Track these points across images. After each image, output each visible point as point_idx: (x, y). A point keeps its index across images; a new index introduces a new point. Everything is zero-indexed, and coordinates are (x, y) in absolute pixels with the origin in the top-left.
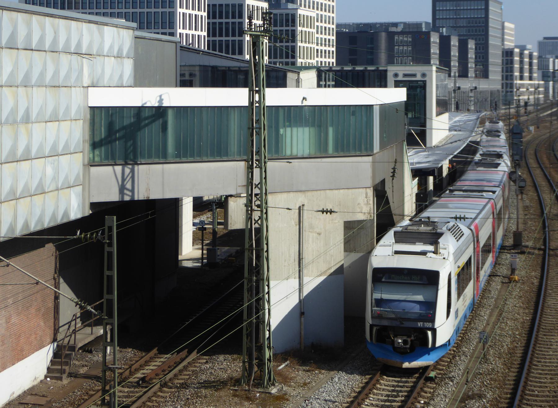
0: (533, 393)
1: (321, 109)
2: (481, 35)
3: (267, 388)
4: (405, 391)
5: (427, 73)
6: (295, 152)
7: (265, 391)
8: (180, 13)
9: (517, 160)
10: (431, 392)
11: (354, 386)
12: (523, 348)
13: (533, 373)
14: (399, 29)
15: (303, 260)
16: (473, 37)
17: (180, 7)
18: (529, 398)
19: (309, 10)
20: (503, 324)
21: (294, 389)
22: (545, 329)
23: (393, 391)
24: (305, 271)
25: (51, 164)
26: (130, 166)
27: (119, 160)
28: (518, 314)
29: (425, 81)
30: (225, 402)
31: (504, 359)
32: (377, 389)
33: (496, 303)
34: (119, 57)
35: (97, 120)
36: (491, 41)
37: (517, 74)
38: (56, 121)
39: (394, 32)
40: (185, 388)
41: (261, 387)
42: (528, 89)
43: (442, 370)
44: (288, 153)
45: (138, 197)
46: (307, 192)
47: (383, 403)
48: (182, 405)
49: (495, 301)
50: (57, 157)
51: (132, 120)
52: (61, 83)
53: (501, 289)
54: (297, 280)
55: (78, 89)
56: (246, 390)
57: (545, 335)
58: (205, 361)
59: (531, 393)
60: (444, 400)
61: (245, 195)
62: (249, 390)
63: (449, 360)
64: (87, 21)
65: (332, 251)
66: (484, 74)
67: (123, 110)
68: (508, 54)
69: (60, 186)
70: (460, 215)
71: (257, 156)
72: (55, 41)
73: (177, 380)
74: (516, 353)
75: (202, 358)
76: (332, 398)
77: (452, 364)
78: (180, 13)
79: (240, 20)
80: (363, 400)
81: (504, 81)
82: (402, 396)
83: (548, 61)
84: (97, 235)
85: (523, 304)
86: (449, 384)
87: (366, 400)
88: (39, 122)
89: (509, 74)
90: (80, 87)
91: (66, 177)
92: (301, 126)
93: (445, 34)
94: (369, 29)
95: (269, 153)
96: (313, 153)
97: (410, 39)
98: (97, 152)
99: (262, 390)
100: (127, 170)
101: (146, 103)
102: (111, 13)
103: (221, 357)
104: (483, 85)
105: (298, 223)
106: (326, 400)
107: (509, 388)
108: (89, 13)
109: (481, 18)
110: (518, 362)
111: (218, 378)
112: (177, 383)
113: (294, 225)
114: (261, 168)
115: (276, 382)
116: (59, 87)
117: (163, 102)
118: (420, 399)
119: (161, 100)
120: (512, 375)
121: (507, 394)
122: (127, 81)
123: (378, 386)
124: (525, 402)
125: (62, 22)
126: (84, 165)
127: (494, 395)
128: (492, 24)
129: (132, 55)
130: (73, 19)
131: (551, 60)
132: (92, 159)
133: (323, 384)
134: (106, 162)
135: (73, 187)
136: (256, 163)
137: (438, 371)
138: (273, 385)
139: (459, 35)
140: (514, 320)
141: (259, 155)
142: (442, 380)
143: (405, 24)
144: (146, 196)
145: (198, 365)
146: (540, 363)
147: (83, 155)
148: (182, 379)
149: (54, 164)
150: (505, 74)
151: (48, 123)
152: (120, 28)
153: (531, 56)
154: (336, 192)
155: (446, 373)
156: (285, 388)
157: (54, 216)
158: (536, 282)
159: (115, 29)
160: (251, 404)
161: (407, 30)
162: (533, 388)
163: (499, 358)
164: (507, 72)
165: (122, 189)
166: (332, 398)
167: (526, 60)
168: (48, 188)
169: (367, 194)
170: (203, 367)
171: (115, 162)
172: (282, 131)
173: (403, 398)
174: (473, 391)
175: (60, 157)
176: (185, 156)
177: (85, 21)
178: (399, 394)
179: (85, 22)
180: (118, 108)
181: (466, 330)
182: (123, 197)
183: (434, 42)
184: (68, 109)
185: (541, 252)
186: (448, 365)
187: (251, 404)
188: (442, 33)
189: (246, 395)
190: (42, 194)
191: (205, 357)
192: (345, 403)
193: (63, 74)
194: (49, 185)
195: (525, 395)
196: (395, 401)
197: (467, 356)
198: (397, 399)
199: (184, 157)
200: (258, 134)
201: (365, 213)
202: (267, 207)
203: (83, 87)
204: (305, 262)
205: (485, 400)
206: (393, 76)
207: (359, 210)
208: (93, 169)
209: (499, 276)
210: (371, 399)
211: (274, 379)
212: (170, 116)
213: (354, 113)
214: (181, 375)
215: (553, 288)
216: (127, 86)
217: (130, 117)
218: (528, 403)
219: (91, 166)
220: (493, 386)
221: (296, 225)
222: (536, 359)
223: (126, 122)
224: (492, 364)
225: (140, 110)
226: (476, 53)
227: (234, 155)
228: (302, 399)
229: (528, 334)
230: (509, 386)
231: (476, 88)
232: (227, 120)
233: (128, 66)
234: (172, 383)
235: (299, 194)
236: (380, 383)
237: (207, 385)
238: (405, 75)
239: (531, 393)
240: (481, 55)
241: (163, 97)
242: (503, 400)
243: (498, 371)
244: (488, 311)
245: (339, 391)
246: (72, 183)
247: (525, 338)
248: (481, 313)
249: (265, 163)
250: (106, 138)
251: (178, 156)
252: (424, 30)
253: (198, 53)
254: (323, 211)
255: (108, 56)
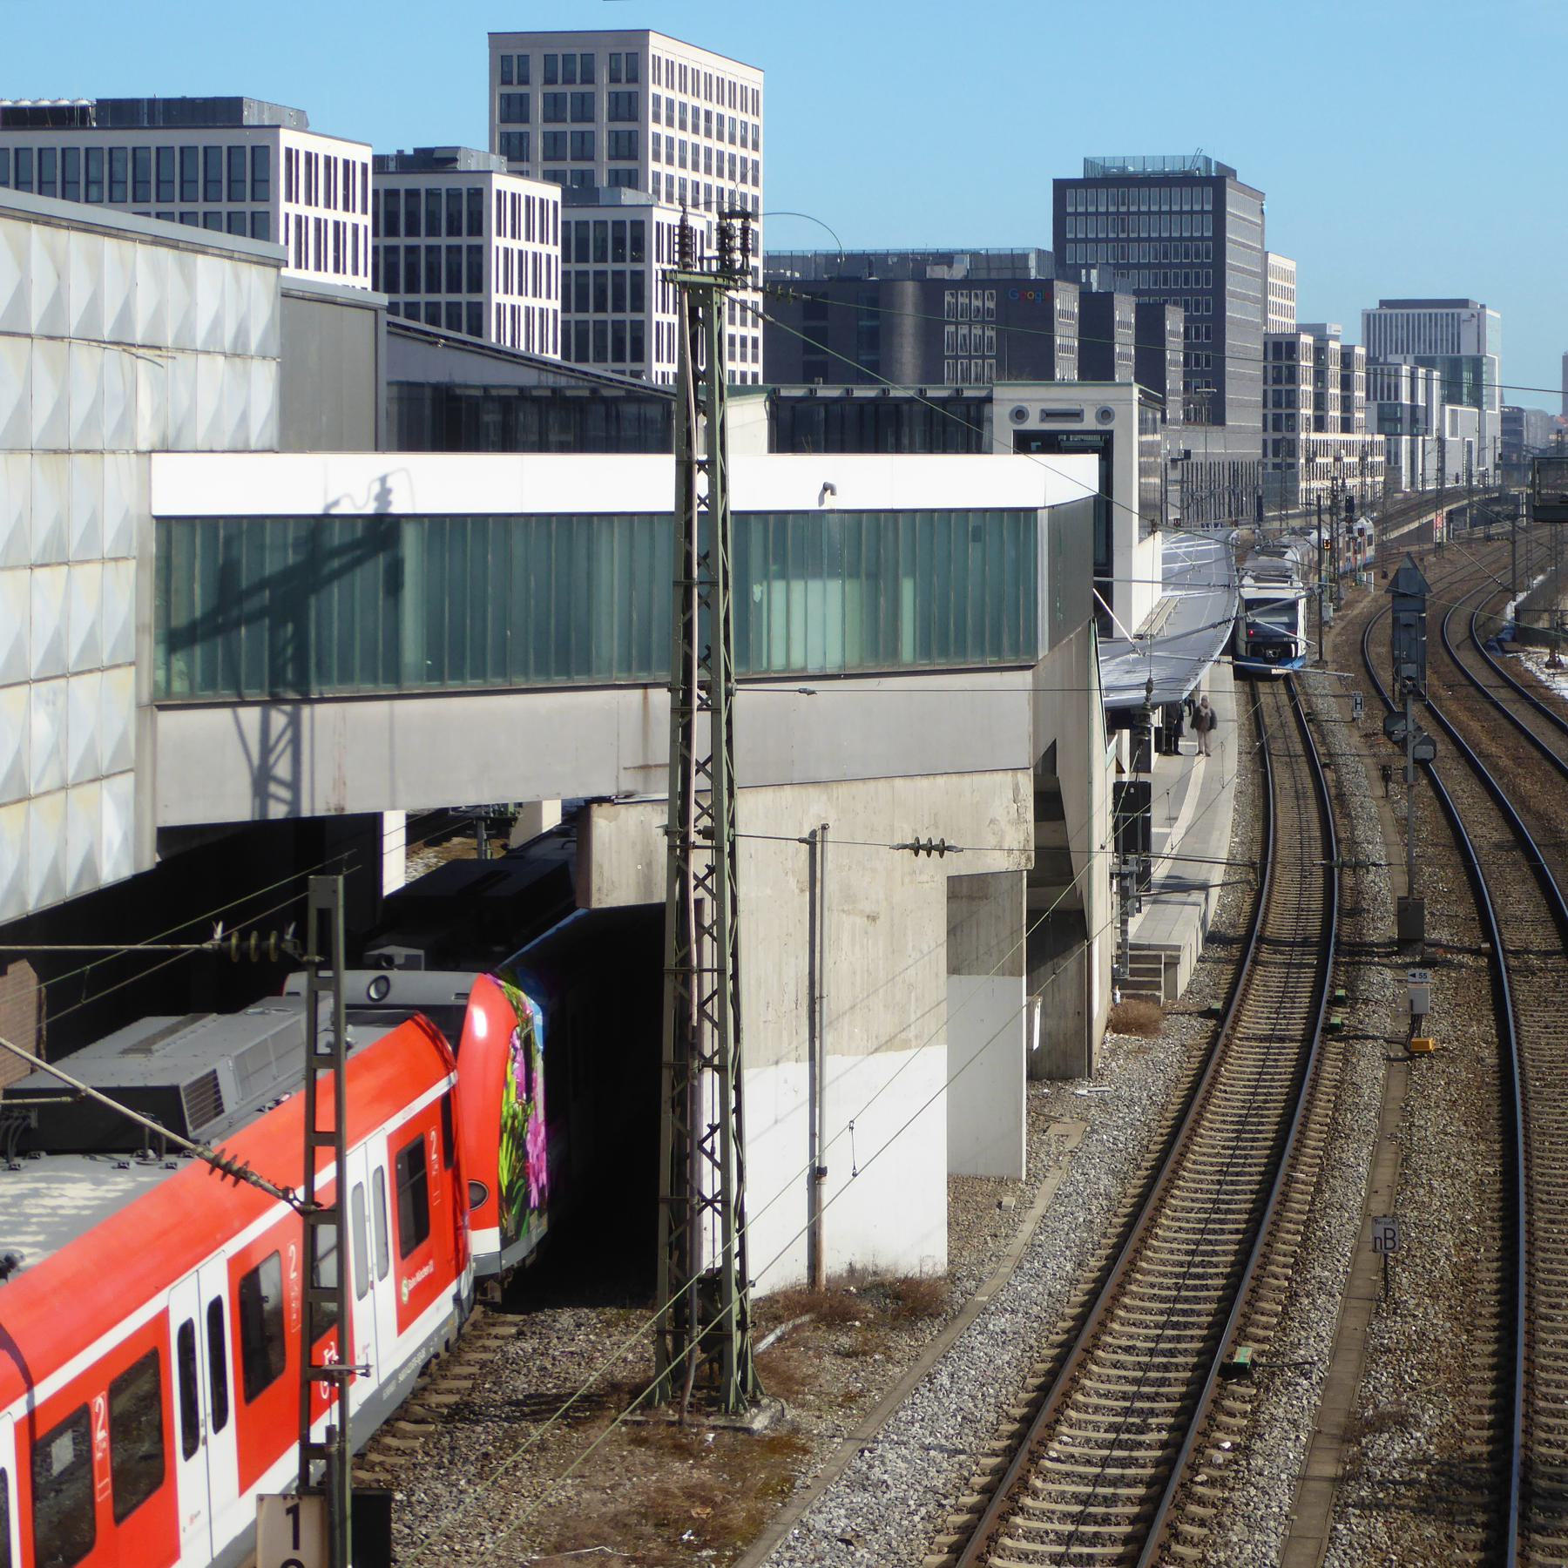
0: (1559, 1406)
1: (878, 520)
2: (1202, 292)
3: (736, 1413)
4: (1165, 1412)
5: (1117, 409)
6: (797, 660)
7: (732, 1424)
8: (287, 216)
9: (1409, 678)
10: (1246, 1412)
11: (1002, 1399)
12: (1495, 1264)
13: (1545, 1342)
14: (959, 271)
15: (825, 1000)
16: (1175, 297)
17: (289, 199)
18: (1552, 1421)
19: (669, 206)
20: (1422, 1192)
21: (817, 1413)
22: (1550, 1202)
23: (1127, 1412)
24: (829, 1038)
25: (47, 703)
26: (288, 708)
27: (248, 687)
28: (1460, 1156)
29: (1111, 433)
30: (609, 1461)
31: (1449, 1299)
32: (1077, 1407)
33: (1382, 1123)
34: (239, 356)
35: (179, 559)
36: (1234, 311)
37: (1306, 411)
38: (60, 564)
39: (943, 280)
40: (464, 1420)
41: (719, 1410)
42: (1338, 459)
43: (1266, 1340)
44: (778, 661)
45: (313, 810)
46: (834, 785)
47: (1106, 1452)
48: (470, 1476)
49: (1378, 1116)
50: (62, 682)
51: (291, 559)
52: (75, 440)
53: (1387, 1078)
54: (806, 1065)
55: (121, 457)
56: (671, 1424)
57: (1552, 1222)
58: (513, 1330)
59: (1552, 1406)
60: (1293, 1437)
61: (666, 796)
62: (680, 1422)
63: (1280, 1308)
64: (149, 238)
65: (911, 971)
66: (1212, 411)
67: (263, 528)
68: (1281, 350)
69: (71, 773)
70: (930, 840)
71: (704, 671)
72: (58, 302)
73: (435, 1395)
74: (1481, 1282)
75: (502, 1319)
76: (943, 1442)
77: (1292, 1319)
78: (287, 216)
79: (475, 241)
80: (1042, 1443)
81: (1272, 435)
82: (1160, 1429)
83: (1398, 375)
84: (281, 938)
85: (1465, 1124)
86: (1298, 1384)
87: (1050, 1444)
88: (12, 568)
89: (1284, 411)
90: (128, 452)
91: (91, 749)
92: (817, 575)
93: (1095, 287)
94: (867, 270)
95: (738, 663)
96: (853, 666)
97: (991, 305)
98: (179, 664)
99: (721, 1422)
100: (279, 719)
101: (336, 503)
102: (205, 214)
103: (566, 1318)
104: (1210, 446)
105: (807, 885)
106: (927, 1448)
107: (1482, 1391)
108: (158, 216)
109: (1202, 238)
110: (1493, 1310)
111: (568, 1385)
112: (438, 1406)
113: (797, 891)
114: (716, 712)
115: (762, 1393)
116: (68, 452)
117: (392, 497)
118: (1219, 1435)
119: (384, 495)
120: (1483, 1351)
121: (1481, 1413)
122: (261, 434)
123: (1080, 1397)
124: (1543, 1435)
125: (76, 241)
126: (139, 706)
127: (1441, 1414)
128: (1233, 258)
129: (274, 349)
130: (108, 231)
131: (1405, 370)
132: (162, 684)
133: (904, 1396)
134: (208, 696)
135: (107, 777)
136: (699, 697)
137: (1256, 1346)
138: (755, 1403)
139: (1137, 293)
140: (1452, 1177)
141: (709, 669)
142: (1273, 1374)
143: (975, 255)
144: (333, 802)
145: (493, 1343)
146: (1557, 1311)
147: (138, 675)
148: (450, 1391)
149: (54, 704)
150: (1271, 412)
151: (38, 572)
152: (240, 260)
153: (1347, 357)
154: (924, 783)
155: (1281, 1350)
156: (790, 1414)
157: (55, 874)
158: (1490, 1056)
159: (227, 262)
160: (692, 1467)
161: (983, 275)
162: (1553, 1390)
163: (1430, 1296)
164: (1277, 404)
165: (262, 779)
166: (943, 1442)
167: (1334, 369)
168: (38, 783)
169: (1016, 790)
170: (511, 1349)
171: (240, 695)
172: (757, 591)
173: (1164, 1435)
174: (1376, 1407)
175: (73, 680)
176: (458, 674)
177: (143, 237)
178: (1150, 1421)
179: (142, 242)
180: (245, 521)
181: (1310, 1211)
182: (264, 807)
183: (1064, 314)
184: (94, 525)
185: (1484, 962)
186: (1279, 1324)
187: (692, 1467)
188: (1089, 283)
189: (673, 1438)
190: (19, 801)
191: (510, 1318)
192: (987, 1455)
193: (80, 409)
194: (40, 776)
195: (1536, 1412)
196: (1139, 1445)
197: (1334, 1296)
198: (1147, 1438)
199: (452, 678)
200: (708, 603)
201: (1010, 850)
202: (734, 836)
203: (137, 452)
204: (829, 1007)
205: (1419, 1434)
206: (1011, 418)
207: (992, 841)
208: (167, 719)
209: (1374, 1038)
210: (1065, 1439)
211: (756, 1385)
212: (411, 546)
213: (978, 535)
214: (444, 1377)
215: (1543, 1073)
216: (259, 448)
217: (285, 547)
218: (1552, 1437)
219: (161, 708)
220: (1433, 1387)
221: (802, 891)
222: (1543, 1298)
223: (272, 565)
224: (1415, 1316)
225: (317, 525)
226: (1188, 348)
227: (610, 671)
228: (851, 1447)
229: (1502, 1219)
230: (1480, 1387)
231: (1187, 454)
232: (590, 558)
233: (264, 380)
234: (422, 1406)
235: (812, 792)
236: (1083, 1388)
237: (538, 1406)
238: (1048, 415)
239: (1552, 1406)
240: (1203, 354)
241: (390, 483)
242: (1471, 1432)
243: (1436, 1340)
244: (1365, 1151)
245: (959, 1419)
246: (105, 766)
247: (1497, 1234)
248: (1344, 1155)
249: (729, 693)
250: (209, 616)
251: (435, 673)
252: (1033, 274)
253: (431, 343)
254: (916, 848)
255: (208, 352)
